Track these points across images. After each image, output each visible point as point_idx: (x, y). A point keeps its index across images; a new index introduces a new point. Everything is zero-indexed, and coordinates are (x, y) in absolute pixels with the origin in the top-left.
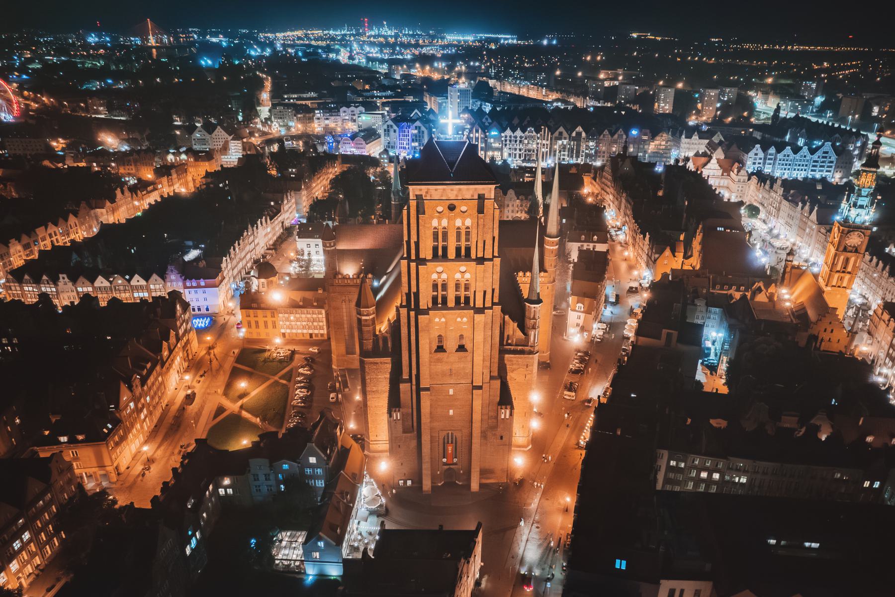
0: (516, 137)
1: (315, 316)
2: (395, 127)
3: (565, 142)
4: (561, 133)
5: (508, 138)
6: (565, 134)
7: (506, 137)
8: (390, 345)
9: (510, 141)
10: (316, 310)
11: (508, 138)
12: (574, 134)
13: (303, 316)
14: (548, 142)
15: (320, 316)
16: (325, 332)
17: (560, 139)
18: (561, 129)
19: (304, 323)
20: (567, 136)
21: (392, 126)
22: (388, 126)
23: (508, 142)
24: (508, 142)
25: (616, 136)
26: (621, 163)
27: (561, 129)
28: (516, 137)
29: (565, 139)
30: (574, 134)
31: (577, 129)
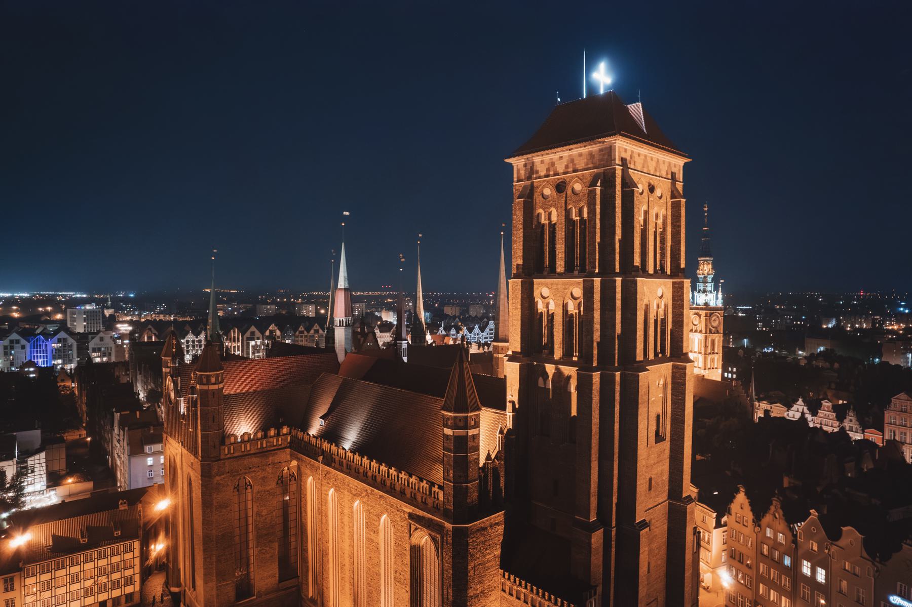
0: (200, 341)
1: (116, 559)
2: (23, 342)
3: (259, 342)
4: (253, 333)
5: (191, 343)
6: (258, 334)
7: (188, 342)
8: (502, 485)
9: (193, 346)
10: (121, 546)
11: (191, 343)
12: (267, 333)
13: (89, 566)
14: (240, 344)
15: (128, 556)
16: (137, 588)
17: (253, 339)
18: (253, 329)
19: (89, 583)
20: (261, 336)
21: (18, 342)
22: (11, 341)
23: (190, 348)
24: (190, 348)
25: (312, 332)
26: (362, 339)
27: (253, 329)
28: (200, 341)
29: (258, 339)
30: (267, 333)
31: (271, 328)
